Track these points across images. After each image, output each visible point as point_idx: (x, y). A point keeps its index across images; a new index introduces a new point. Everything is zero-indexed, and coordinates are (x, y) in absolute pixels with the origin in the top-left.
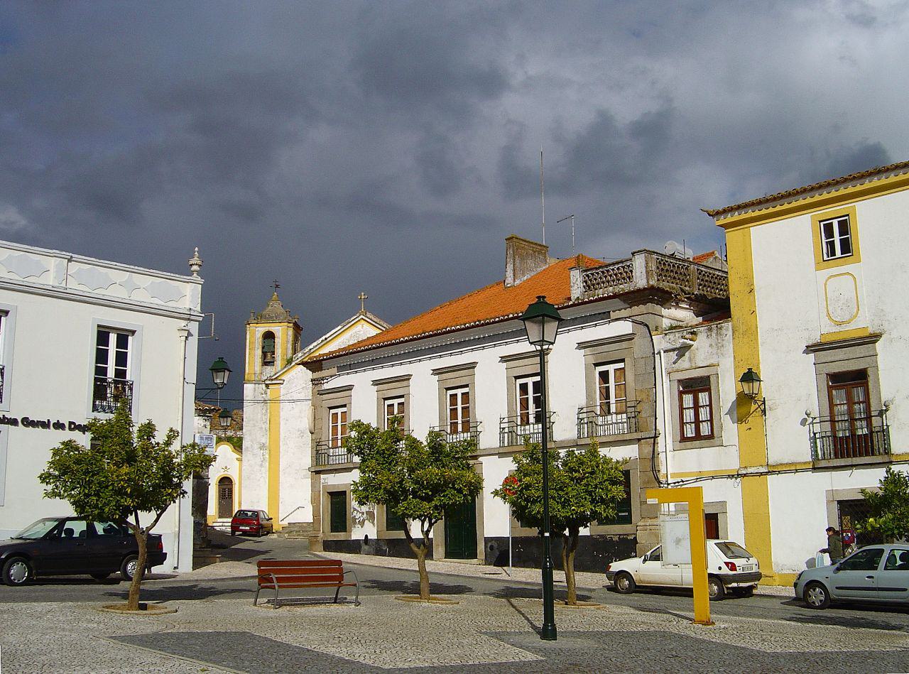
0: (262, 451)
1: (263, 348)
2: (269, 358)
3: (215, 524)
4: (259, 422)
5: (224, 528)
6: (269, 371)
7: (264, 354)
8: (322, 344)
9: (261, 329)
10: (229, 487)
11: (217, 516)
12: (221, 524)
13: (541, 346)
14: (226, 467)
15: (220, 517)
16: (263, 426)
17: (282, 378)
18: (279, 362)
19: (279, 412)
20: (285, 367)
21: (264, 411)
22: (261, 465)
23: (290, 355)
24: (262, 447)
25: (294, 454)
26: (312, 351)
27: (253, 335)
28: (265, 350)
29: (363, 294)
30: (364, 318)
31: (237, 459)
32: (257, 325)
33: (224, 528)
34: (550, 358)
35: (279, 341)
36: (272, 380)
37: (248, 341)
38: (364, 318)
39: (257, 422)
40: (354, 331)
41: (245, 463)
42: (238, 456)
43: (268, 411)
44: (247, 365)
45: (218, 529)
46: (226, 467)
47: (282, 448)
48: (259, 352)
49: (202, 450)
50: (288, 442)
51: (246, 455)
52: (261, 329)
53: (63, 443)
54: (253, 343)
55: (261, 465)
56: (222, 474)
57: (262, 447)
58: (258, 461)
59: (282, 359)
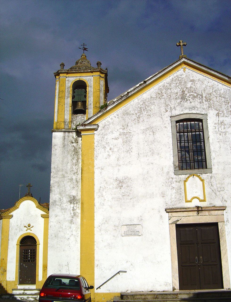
0: (72, 205)
1: (73, 97)
2: (80, 106)
3: (15, 292)
4: (69, 172)
5: (25, 297)
6: (80, 118)
7: (74, 104)
8: (141, 87)
9: (72, 79)
10: (31, 247)
11: (17, 282)
12: (22, 292)
13: (188, 131)
14: (29, 226)
15: (21, 283)
16: (74, 177)
17: (97, 123)
18: (91, 111)
19: (93, 161)
20: (100, 112)
21: (74, 161)
22: (71, 222)
23: (102, 104)
24: (73, 200)
25: (111, 207)
26: (130, 94)
27: (62, 85)
28: (75, 99)
29: (181, 41)
30: (186, 61)
31: (42, 216)
32: (67, 76)
33: (25, 297)
34: (223, 132)
35: (90, 90)
36: (85, 125)
37: (57, 91)
38: (186, 61)
39: (66, 173)
40: (175, 75)
41: (52, 220)
42: (44, 213)
43: (80, 161)
44: (56, 114)
45: (18, 298)
46: (29, 226)
47: (97, 201)
48: (69, 101)
49: (74, 204)
50: (104, 194)
51: (54, 211)
52: (72, 79)
53: (12, 216)
54: (63, 91)
55: (71, 222)
56: (24, 232)
57: (73, 200)
58: (68, 216)
59: (95, 107)
